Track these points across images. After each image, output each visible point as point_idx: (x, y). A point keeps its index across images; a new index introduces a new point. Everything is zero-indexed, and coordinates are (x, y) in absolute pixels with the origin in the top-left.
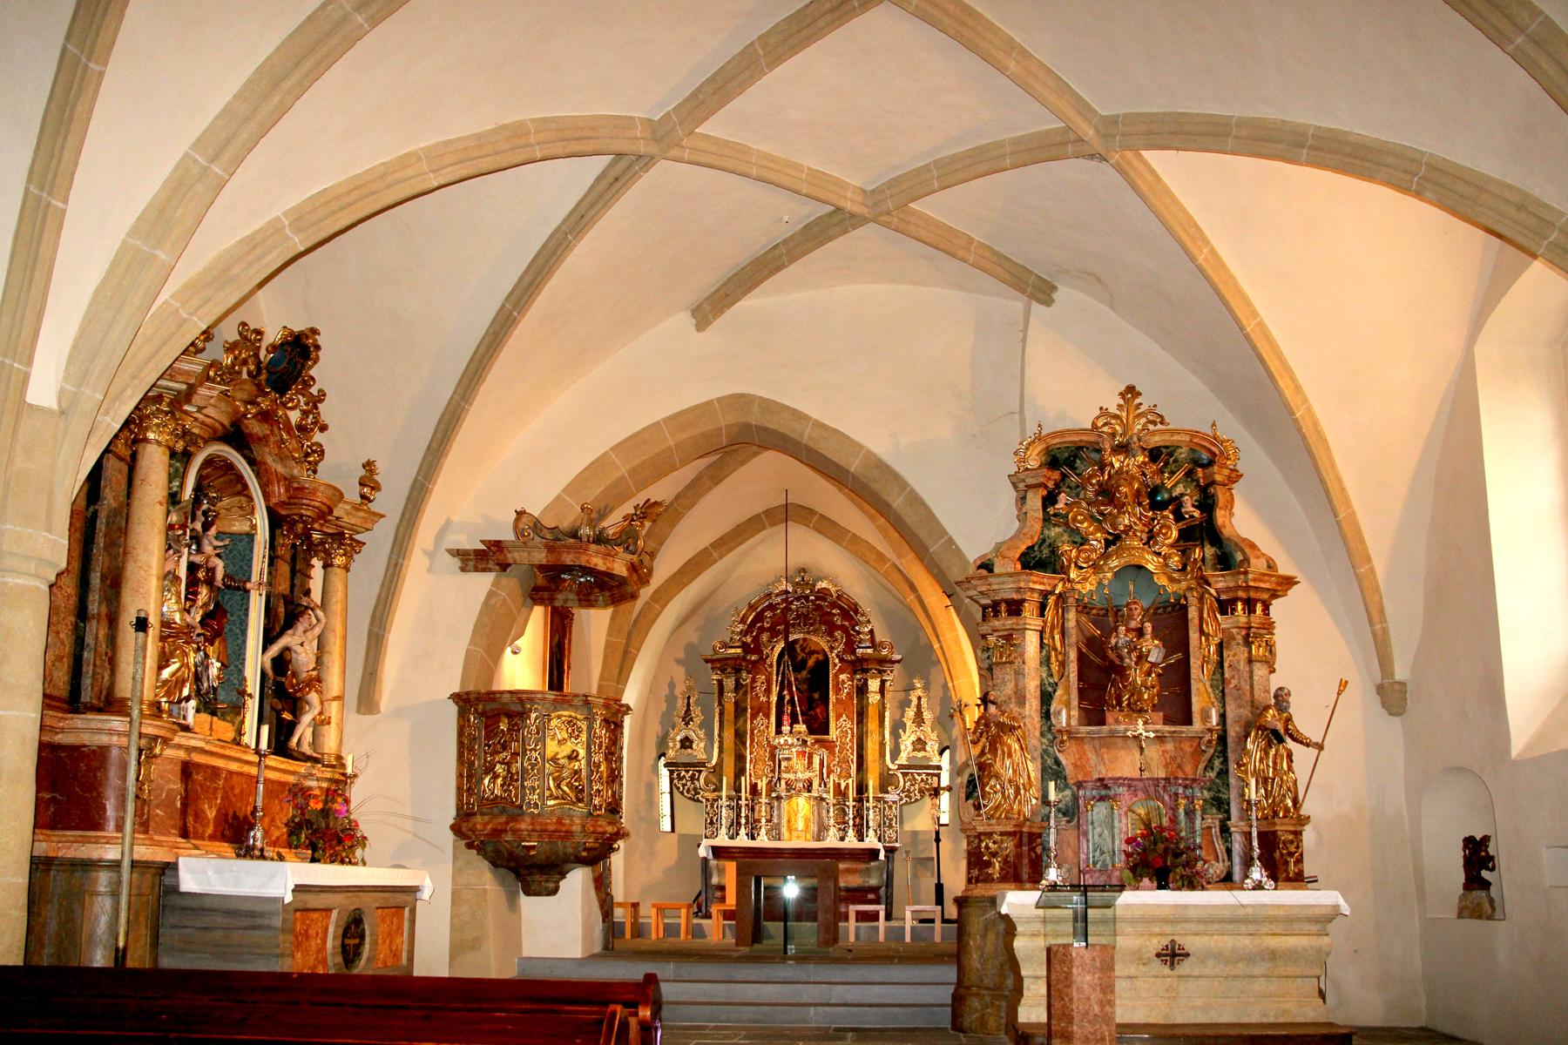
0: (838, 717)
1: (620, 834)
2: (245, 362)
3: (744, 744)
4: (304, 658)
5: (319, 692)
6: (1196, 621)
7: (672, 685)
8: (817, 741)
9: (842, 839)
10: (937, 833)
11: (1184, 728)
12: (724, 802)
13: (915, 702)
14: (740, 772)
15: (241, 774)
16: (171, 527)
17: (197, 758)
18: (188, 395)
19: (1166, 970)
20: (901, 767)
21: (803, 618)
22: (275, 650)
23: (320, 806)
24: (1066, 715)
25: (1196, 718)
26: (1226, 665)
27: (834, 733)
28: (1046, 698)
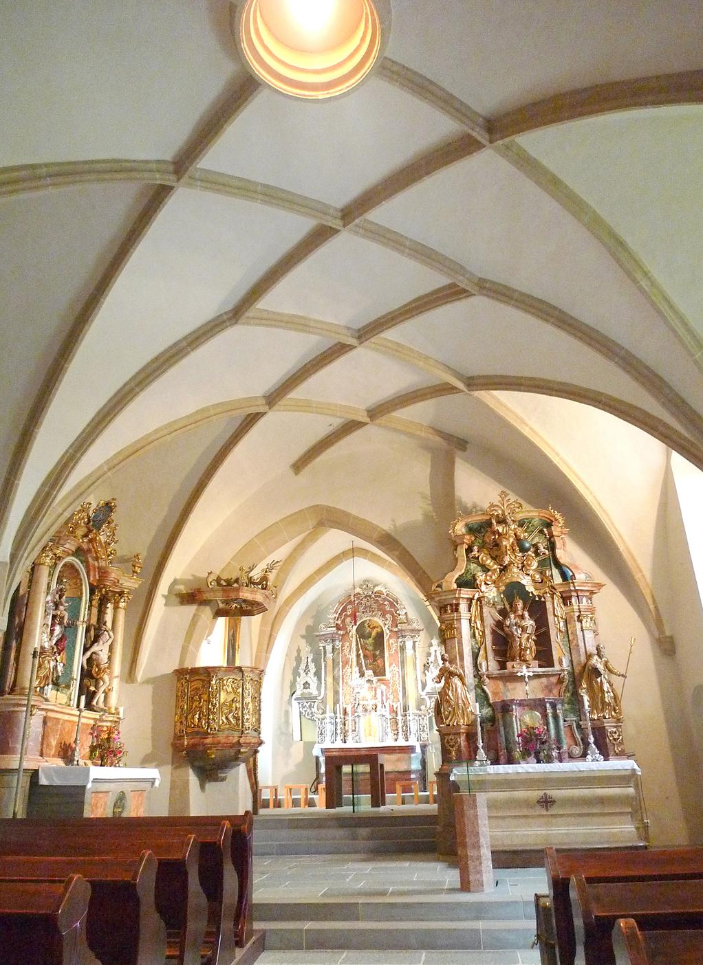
0: (390, 666)
1: (261, 743)
2: (83, 518)
3: (338, 684)
4: (104, 656)
5: (108, 674)
6: (551, 609)
7: (299, 651)
8: (379, 680)
9: (396, 740)
14: (336, 702)
15: (69, 721)
16: (47, 602)
17: (51, 714)
19: (544, 812)
20: (428, 694)
21: (369, 609)
22: (88, 654)
23: (106, 736)
24: (490, 665)
26: (570, 632)
27: (388, 675)
28: (475, 656)
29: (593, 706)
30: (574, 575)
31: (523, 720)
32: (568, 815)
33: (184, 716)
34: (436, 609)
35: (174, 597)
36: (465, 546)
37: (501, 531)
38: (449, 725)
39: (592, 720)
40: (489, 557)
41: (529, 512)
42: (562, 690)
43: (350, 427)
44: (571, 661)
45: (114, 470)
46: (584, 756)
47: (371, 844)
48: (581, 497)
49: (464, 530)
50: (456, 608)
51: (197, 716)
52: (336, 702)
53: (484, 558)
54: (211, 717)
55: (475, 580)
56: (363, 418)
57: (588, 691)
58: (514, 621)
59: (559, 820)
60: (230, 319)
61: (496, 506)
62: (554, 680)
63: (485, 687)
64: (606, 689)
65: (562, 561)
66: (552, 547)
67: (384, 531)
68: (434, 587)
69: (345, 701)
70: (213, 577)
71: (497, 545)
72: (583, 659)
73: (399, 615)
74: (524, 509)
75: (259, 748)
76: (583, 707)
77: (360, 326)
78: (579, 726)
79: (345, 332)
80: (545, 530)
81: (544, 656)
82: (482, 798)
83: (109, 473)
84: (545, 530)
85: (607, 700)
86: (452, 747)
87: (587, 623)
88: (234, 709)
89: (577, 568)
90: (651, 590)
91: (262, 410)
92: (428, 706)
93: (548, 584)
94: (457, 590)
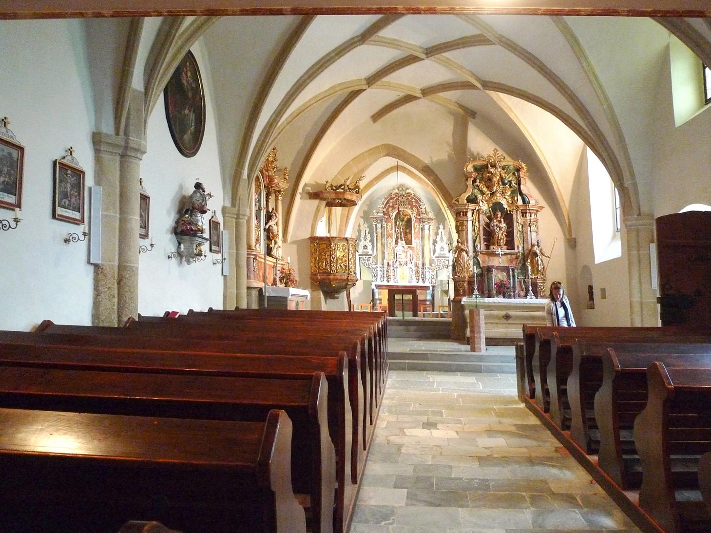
0: (415, 238)
3: (384, 247)
7: (359, 226)
8: (408, 247)
9: (418, 282)
10: (448, 281)
11: (513, 251)
12: (379, 269)
13: (440, 234)
14: (383, 258)
18: (653, 451)
19: (505, 322)
21: (403, 203)
24: (481, 247)
25: (516, 248)
27: (414, 244)
28: (474, 241)
29: (532, 271)
30: (529, 201)
31: (497, 276)
32: (517, 324)
33: (317, 262)
34: (453, 214)
35: (306, 194)
36: (472, 179)
37: (493, 172)
38: (459, 277)
39: (531, 279)
40: (485, 186)
41: (509, 162)
42: (518, 263)
43: (409, 98)
44: (524, 247)
45: (290, 124)
46: (526, 296)
47: (419, 334)
48: (535, 153)
49: (472, 170)
50: (465, 214)
51: (324, 263)
52: (383, 258)
53: (482, 187)
54: (332, 264)
55: (477, 199)
56: (419, 95)
57: (530, 265)
58: (495, 224)
59: (512, 326)
60: (359, 41)
61: (491, 156)
62: (514, 257)
63: (478, 258)
64: (539, 264)
65: (523, 192)
66: (519, 183)
67: (426, 164)
68: (453, 201)
69: (389, 258)
70: (329, 184)
71: (490, 179)
72: (530, 247)
73: (421, 209)
74: (506, 160)
75: (356, 283)
76: (528, 272)
77: (428, 47)
78: (524, 281)
79: (421, 50)
80: (516, 173)
81: (510, 244)
82: (482, 312)
83: (288, 126)
84: (516, 173)
85: (539, 269)
86: (461, 288)
87: (533, 228)
88: (344, 261)
89: (531, 197)
90: (568, 213)
91: (364, 87)
92: (436, 264)
93: (515, 204)
94: (466, 204)
